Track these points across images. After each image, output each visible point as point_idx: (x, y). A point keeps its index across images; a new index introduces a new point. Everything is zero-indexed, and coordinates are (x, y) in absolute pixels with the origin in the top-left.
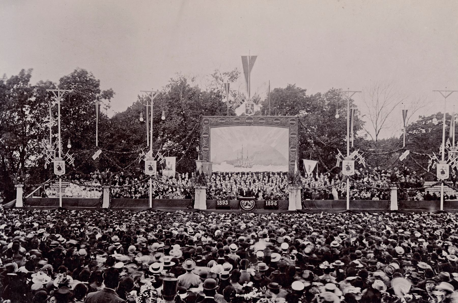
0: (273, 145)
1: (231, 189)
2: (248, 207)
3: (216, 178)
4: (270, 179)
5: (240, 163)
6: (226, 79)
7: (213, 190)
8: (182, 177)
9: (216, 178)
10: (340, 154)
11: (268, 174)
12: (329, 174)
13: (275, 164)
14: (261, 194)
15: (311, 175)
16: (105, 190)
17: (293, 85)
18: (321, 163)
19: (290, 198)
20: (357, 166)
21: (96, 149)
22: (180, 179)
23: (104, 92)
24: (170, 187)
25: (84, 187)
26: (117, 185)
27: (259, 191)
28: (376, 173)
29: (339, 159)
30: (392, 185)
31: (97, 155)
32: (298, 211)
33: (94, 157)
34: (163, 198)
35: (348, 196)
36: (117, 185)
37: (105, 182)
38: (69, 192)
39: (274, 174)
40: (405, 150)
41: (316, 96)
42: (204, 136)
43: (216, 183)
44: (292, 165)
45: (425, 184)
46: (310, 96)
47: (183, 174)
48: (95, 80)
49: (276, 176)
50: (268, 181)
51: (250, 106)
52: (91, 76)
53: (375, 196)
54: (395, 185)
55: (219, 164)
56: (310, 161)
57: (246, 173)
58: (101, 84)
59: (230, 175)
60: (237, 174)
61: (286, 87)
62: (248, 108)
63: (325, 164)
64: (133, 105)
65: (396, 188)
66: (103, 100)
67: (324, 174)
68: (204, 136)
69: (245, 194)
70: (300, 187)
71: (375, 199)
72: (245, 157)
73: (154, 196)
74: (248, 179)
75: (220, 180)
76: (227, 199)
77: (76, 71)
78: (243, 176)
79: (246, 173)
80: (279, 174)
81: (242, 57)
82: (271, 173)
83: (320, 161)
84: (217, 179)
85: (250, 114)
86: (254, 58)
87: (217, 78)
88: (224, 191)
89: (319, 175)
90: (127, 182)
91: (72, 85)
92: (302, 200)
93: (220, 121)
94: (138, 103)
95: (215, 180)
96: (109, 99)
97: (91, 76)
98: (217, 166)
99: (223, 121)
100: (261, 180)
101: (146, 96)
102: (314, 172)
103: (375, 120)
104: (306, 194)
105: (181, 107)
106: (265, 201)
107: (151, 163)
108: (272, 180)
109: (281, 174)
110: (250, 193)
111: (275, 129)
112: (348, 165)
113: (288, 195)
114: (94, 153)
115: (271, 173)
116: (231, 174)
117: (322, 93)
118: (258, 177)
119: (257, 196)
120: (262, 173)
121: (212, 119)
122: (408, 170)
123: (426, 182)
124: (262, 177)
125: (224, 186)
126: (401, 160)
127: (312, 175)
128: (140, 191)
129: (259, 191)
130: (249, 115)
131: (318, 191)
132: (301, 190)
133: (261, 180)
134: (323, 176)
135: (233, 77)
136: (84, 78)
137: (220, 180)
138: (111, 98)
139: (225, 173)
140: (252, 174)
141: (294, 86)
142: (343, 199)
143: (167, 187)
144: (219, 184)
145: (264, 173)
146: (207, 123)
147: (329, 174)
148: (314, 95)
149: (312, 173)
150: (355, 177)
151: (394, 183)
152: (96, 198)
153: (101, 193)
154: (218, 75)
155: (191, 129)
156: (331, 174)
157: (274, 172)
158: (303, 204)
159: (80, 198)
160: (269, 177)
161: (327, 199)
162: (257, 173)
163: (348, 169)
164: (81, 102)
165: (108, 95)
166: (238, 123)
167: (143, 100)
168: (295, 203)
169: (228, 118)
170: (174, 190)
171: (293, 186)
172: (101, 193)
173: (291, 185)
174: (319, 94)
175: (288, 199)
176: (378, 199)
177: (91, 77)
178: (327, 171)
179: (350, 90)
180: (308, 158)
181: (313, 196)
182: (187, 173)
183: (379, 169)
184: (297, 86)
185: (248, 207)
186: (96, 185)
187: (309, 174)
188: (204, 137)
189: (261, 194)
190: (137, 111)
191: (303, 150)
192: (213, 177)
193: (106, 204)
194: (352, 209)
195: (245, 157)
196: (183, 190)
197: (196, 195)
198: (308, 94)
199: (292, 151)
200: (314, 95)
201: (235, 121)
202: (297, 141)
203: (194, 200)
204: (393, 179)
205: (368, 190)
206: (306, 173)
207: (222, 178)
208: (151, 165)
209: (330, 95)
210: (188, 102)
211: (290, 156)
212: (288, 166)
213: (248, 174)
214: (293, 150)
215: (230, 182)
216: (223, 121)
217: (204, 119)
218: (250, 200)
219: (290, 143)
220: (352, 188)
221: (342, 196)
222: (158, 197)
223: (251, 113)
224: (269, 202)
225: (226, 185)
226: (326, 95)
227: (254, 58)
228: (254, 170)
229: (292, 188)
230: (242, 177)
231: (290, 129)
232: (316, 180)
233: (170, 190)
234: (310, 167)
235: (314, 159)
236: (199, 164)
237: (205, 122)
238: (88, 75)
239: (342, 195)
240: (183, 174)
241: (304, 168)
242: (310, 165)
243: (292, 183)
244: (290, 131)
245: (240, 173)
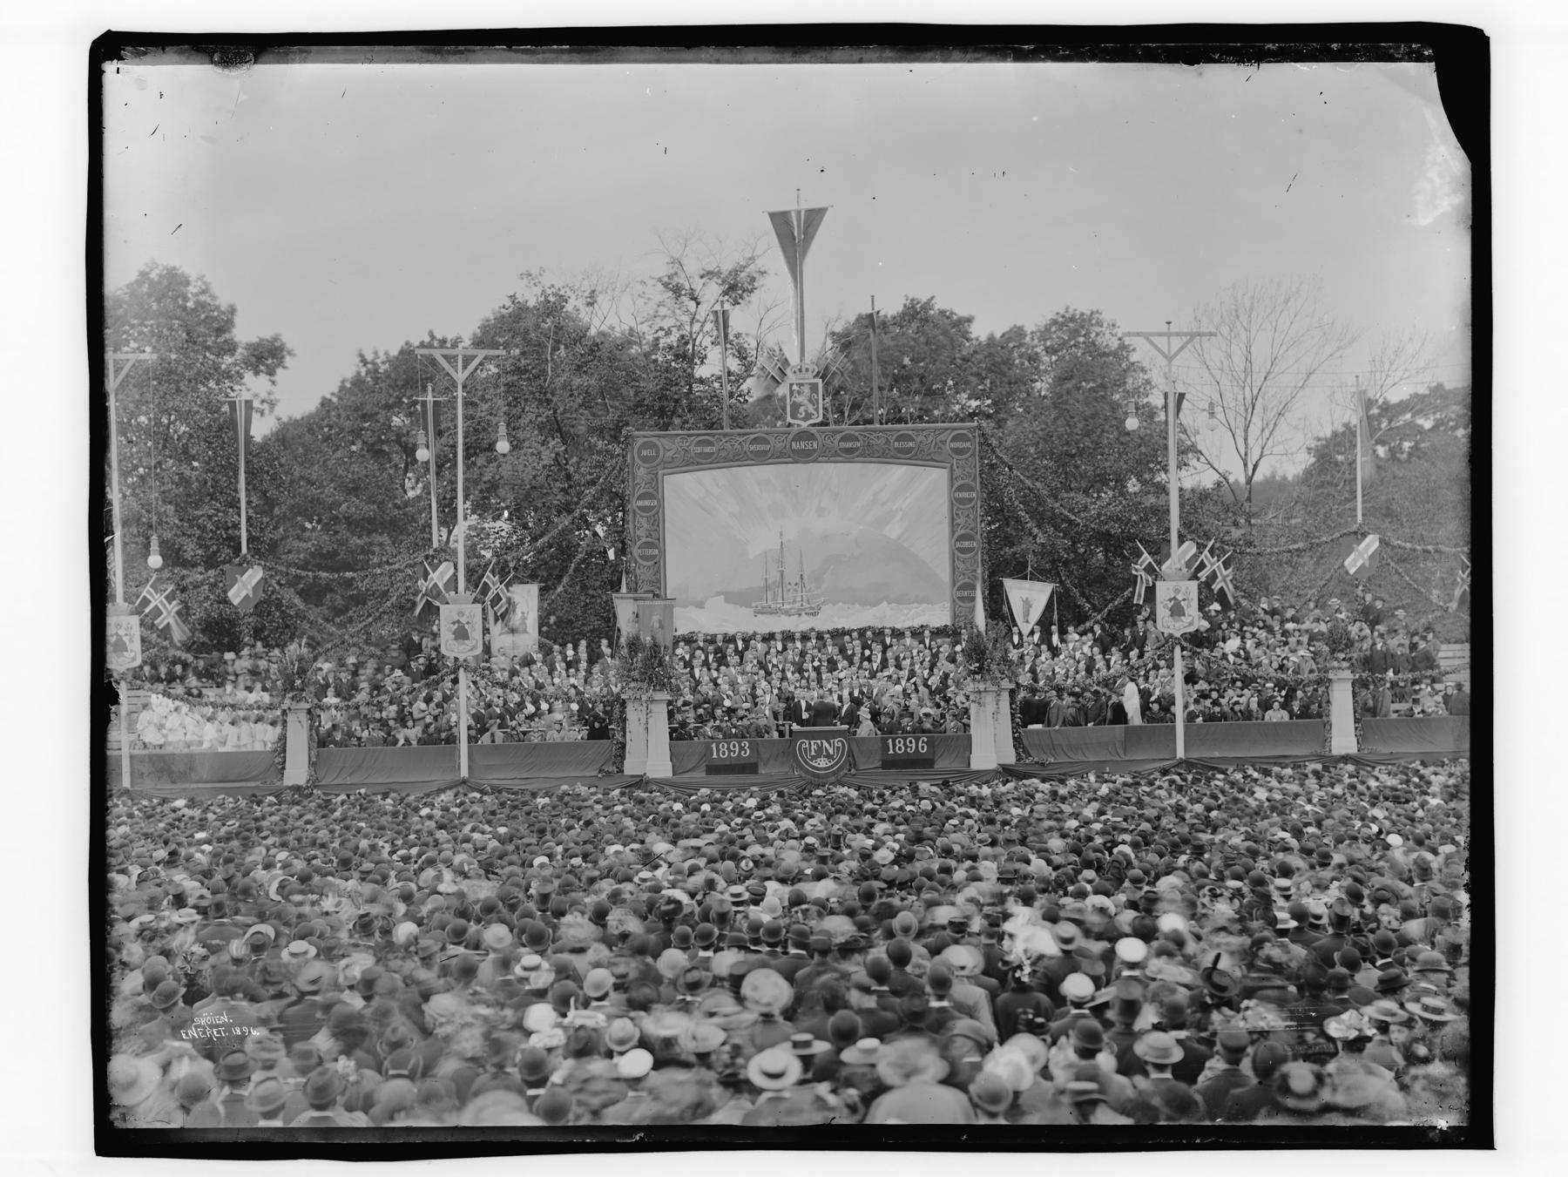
0: (893, 531)
1: (754, 697)
2: (823, 763)
3: (693, 656)
4: (889, 654)
5: (774, 599)
6: (711, 293)
7: (686, 704)
8: (565, 657)
9: (693, 656)
10: (1146, 558)
11: (879, 634)
12: (1097, 629)
13: (902, 600)
14: (864, 712)
15: (1032, 633)
16: (290, 718)
17: (924, 299)
18: (1067, 590)
19: (972, 722)
20: (1207, 594)
21: (240, 564)
22: (560, 666)
23: (249, 347)
24: (528, 699)
25: (209, 710)
26: (331, 699)
27: (857, 702)
28: (1268, 618)
29: (1145, 579)
30: (1335, 664)
31: (245, 586)
32: (1006, 773)
33: (237, 595)
34: (509, 736)
35: (1178, 710)
36: (331, 699)
37: (293, 688)
38: (152, 728)
39: (898, 634)
40: (1364, 535)
41: (1007, 337)
42: (640, 503)
43: (692, 676)
44: (962, 599)
45: (1441, 655)
46: (983, 339)
47: (570, 646)
48: (217, 308)
49: (908, 641)
50: (884, 664)
51: (806, 390)
52: (203, 292)
53: (1276, 705)
54: (1345, 664)
55: (700, 605)
56: (1027, 584)
57: (798, 636)
58: (237, 319)
59: (740, 645)
60: (769, 638)
61: (900, 309)
62: (799, 399)
63: (1083, 594)
64: (342, 388)
65: (1348, 674)
66: (249, 376)
67: (1081, 628)
68: (640, 503)
69: (805, 716)
70: (1007, 685)
71: (1277, 715)
72: (792, 576)
73: (473, 733)
74: (808, 657)
75: (706, 663)
76: (743, 737)
77: (144, 274)
78: (790, 645)
79: (798, 636)
80: (917, 633)
81: (772, 216)
82: (887, 631)
83: (1061, 582)
84: (695, 662)
85: (805, 419)
86: (814, 217)
87: (677, 291)
88: (727, 703)
89: (1063, 632)
90: (365, 685)
91: (133, 326)
92: (1014, 730)
93: (699, 450)
94: (358, 382)
95: (688, 664)
96: (271, 373)
97: (203, 292)
98: (693, 612)
99: (708, 449)
100: (857, 659)
101: (386, 353)
102: (1044, 623)
103: (1242, 426)
104: (1029, 711)
105: (548, 401)
106: (884, 741)
107: (461, 613)
108: (897, 658)
109: (927, 633)
110: (824, 713)
111: (896, 474)
112: (1174, 595)
113: (966, 711)
114: (236, 581)
115: (887, 631)
116: (746, 641)
117: (1029, 329)
118: (842, 650)
119: (853, 720)
120: (855, 635)
121: (671, 443)
122: (1379, 605)
123: (1444, 647)
124: (858, 650)
125: (725, 687)
126: (1352, 571)
127: (1036, 637)
128: (416, 715)
129: (857, 702)
130: (805, 425)
131: (1072, 694)
132: (1012, 693)
133: (857, 659)
134: (1077, 637)
135: (736, 288)
136: (175, 299)
137: (706, 663)
138: (279, 371)
139: (720, 638)
140: (820, 636)
141: (927, 306)
142: (1162, 720)
143: (517, 698)
144: (706, 678)
145: (862, 633)
146: (652, 459)
147: (1097, 629)
148: (998, 335)
149: (1037, 628)
150: (1197, 640)
151: (1342, 656)
152: (258, 747)
153: (279, 729)
154: (681, 280)
155: (593, 483)
156: (1103, 628)
157: (898, 626)
158: (1018, 742)
159: (195, 749)
160: (885, 648)
161: (1103, 722)
162: (838, 634)
163: (1177, 611)
164: (178, 391)
165: (267, 356)
166: (766, 452)
167: (376, 371)
168: (991, 742)
169: (725, 435)
170: (544, 706)
171: (984, 680)
172: (279, 729)
173: (978, 677)
174: (1018, 332)
175: (966, 727)
176: (1284, 715)
177: (203, 298)
178: (1087, 618)
179: (1173, 328)
180: (1020, 571)
181: (1053, 713)
182: (583, 643)
183: (1277, 605)
184: (939, 305)
185: (823, 763)
186: (252, 698)
187: (1025, 632)
188: (640, 508)
189: (864, 712)
190: (357, 409)
191: (998, 545)
192: (679, 651)
193: (297, 772)
194: (1195, 755)
195: (792, 576)
196: (575, 707)
197: (630, 725)
198: (980, 331)
199: (962, 550)
200: (998, 335)
201: (753, 448)
202: (980, 512)
203: (623, 746)
204: (1338, 642)
205: (1247, 682)
206: (1015, 629)
207: (711, 657)
208: (463, 620)
209: (1059, 335)
210: (577, 381)
211: (954, 569)
212: (948, 605)
213: (805, 638)
214: (966, 544)
215: (743, 673)
216: (708, 449)
217: (641, 441)
218: (828, 736)
219: (953, 519)
220: (1190, 678)
221: (1158, 711)
222: (487, 735)
223: (808, 416)
224: (900, 744)
225: (733, 684)
226: (1044, 334)
227: (814, 217)
228: (824, 623)
229: (982, 687)
230: (785, 648)
231: (952, 470)
232: (1055, 652)
233: (531, 709)
234: (1027, 605)
235: (1040, 575)
236: (625, 610)
237: (644, 453)
238: (192, 289)
239: (1155, 707)
240: (570, 646)
241: (1005, 609)
242: (1029, 598)
243: (980, 670)
244: (952, 480)
245: (778, 637)
